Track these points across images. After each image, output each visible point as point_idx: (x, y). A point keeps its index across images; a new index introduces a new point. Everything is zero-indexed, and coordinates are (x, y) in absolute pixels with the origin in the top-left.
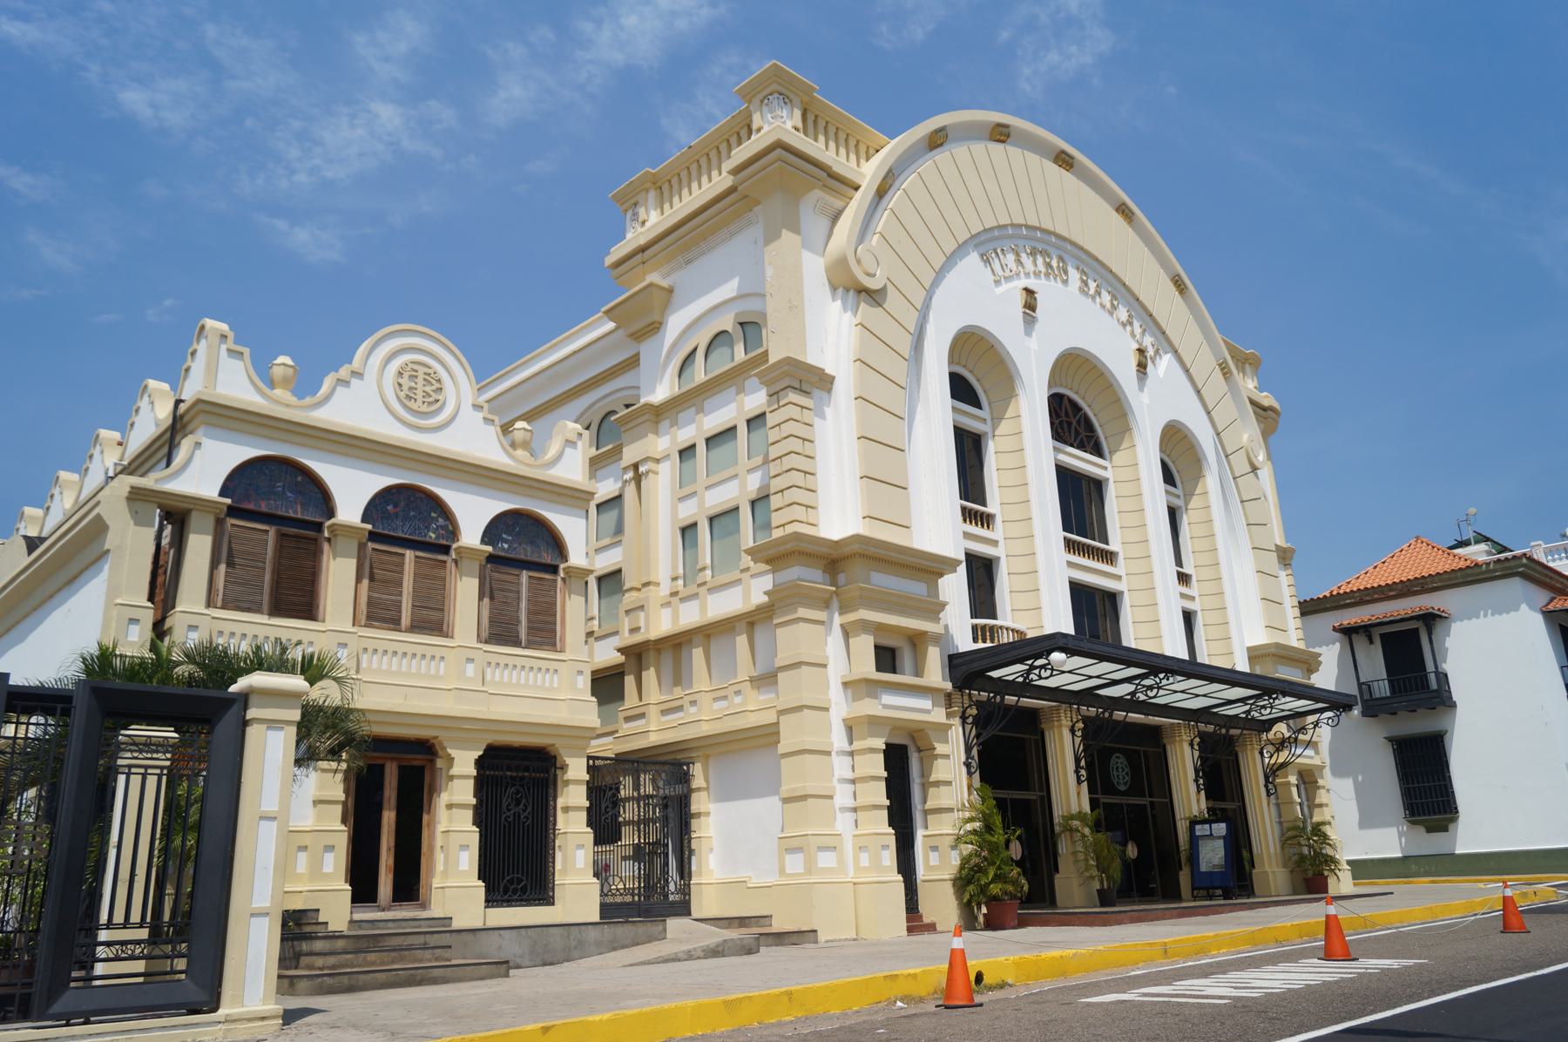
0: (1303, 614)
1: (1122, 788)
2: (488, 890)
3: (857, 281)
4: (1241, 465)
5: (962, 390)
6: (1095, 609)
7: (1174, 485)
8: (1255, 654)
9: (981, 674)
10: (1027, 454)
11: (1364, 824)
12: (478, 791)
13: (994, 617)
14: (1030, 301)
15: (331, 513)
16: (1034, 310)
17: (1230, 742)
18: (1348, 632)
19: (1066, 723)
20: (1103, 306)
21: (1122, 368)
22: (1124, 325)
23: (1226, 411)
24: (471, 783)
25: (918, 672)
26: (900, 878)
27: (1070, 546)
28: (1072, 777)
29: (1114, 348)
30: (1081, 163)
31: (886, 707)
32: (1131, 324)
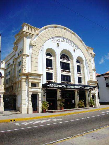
0: (97, 77)
1: (68, 97)
2: (4, 109)
3: (32, 45)
4: (88, 61)
5: (78, 62)
6: (66, 78)
7: (16, 54)
8: (88, 82)
9: (45, 86)
10: (57, 61)
11: (5, 110)
12: (3, 99)
13: (52, 80)
14: (58, 45)
15: (2, 75)
16: (59, 45)
17: (84, 91)
18: (106, 78)
19: (77, 91)
20: (69, 44)
21: (72, 51)
22: (72, 46)
23: (87, 55)
24: (3, 98)
25: (38, 86)
26: (32, 108)
27: (62, 71)
28: (77, 97)
29: (70, 48)
30: (58, 26)
31: (32, 90)
32: (74, 46)
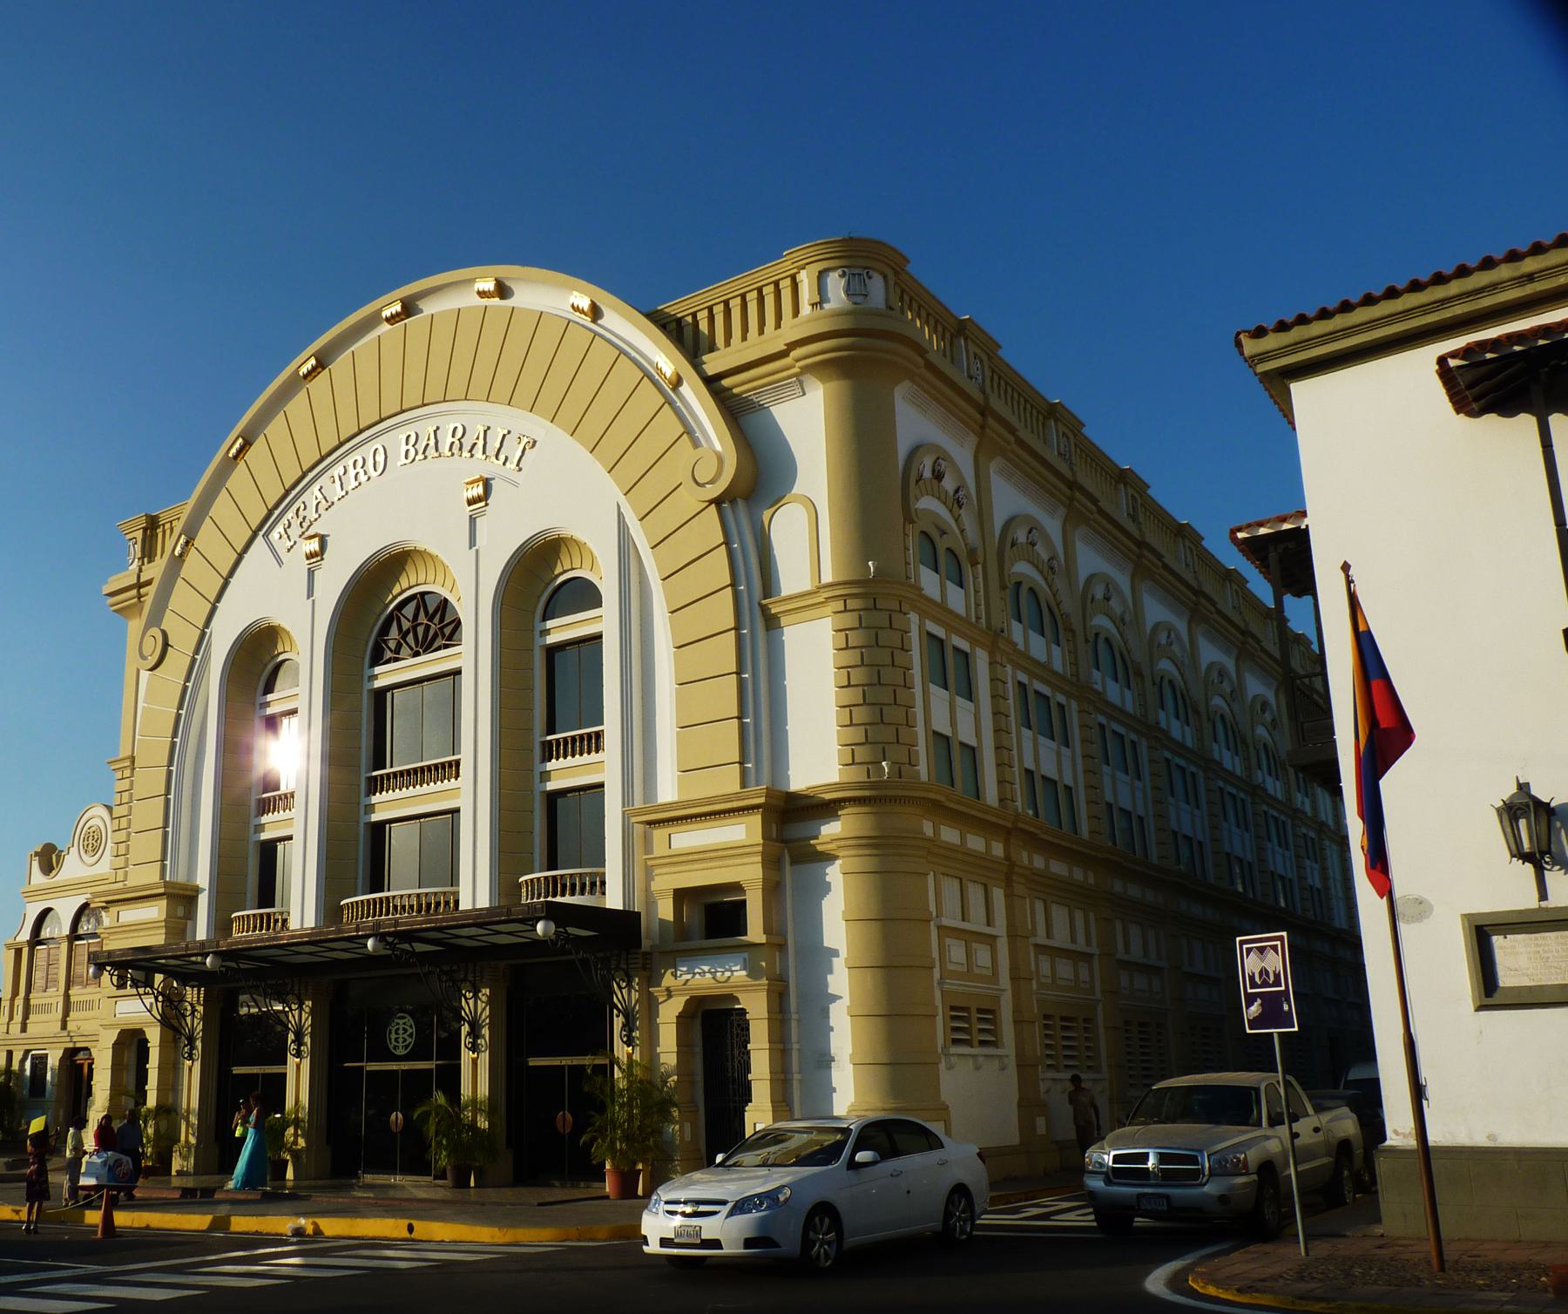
1: (401, 1052)
